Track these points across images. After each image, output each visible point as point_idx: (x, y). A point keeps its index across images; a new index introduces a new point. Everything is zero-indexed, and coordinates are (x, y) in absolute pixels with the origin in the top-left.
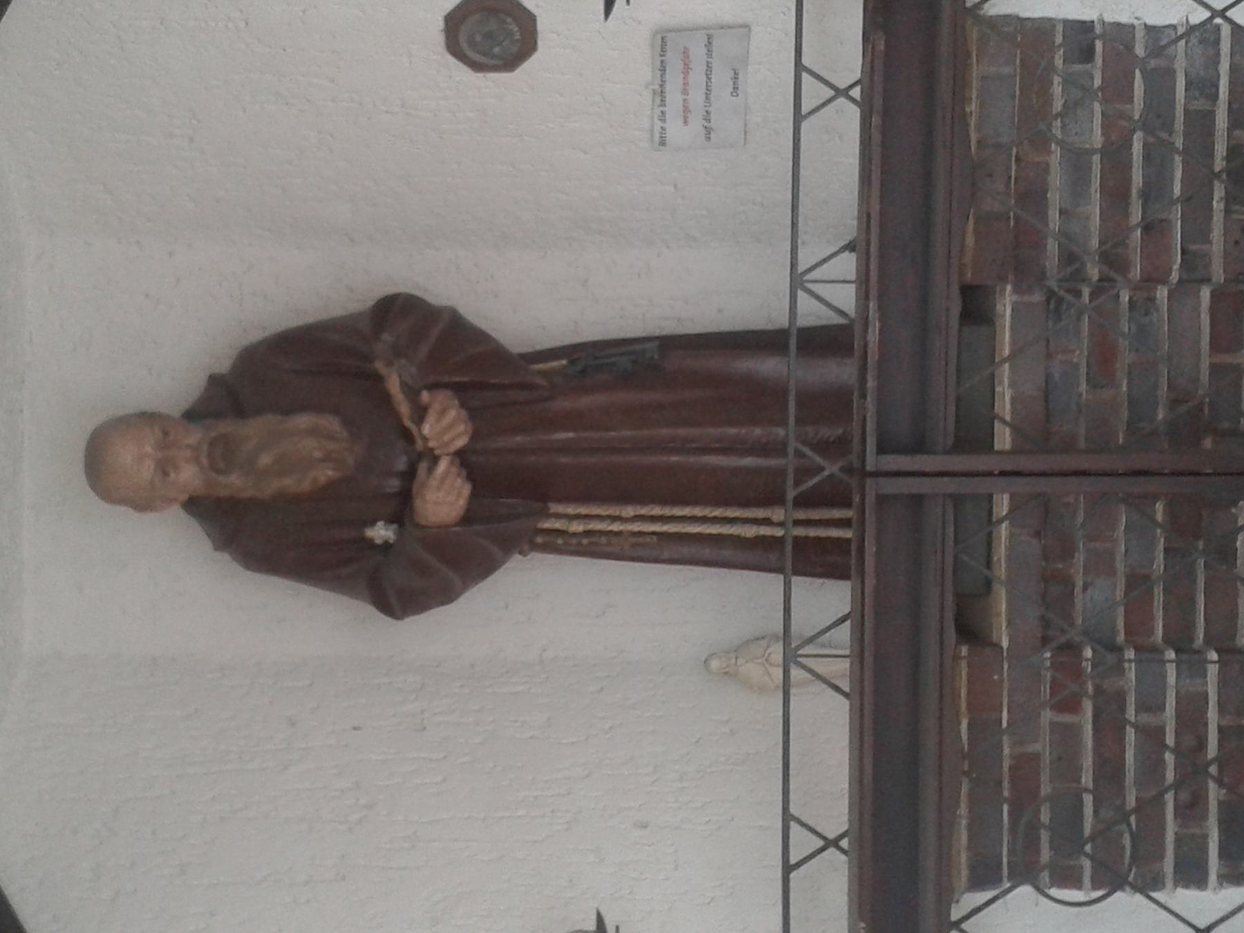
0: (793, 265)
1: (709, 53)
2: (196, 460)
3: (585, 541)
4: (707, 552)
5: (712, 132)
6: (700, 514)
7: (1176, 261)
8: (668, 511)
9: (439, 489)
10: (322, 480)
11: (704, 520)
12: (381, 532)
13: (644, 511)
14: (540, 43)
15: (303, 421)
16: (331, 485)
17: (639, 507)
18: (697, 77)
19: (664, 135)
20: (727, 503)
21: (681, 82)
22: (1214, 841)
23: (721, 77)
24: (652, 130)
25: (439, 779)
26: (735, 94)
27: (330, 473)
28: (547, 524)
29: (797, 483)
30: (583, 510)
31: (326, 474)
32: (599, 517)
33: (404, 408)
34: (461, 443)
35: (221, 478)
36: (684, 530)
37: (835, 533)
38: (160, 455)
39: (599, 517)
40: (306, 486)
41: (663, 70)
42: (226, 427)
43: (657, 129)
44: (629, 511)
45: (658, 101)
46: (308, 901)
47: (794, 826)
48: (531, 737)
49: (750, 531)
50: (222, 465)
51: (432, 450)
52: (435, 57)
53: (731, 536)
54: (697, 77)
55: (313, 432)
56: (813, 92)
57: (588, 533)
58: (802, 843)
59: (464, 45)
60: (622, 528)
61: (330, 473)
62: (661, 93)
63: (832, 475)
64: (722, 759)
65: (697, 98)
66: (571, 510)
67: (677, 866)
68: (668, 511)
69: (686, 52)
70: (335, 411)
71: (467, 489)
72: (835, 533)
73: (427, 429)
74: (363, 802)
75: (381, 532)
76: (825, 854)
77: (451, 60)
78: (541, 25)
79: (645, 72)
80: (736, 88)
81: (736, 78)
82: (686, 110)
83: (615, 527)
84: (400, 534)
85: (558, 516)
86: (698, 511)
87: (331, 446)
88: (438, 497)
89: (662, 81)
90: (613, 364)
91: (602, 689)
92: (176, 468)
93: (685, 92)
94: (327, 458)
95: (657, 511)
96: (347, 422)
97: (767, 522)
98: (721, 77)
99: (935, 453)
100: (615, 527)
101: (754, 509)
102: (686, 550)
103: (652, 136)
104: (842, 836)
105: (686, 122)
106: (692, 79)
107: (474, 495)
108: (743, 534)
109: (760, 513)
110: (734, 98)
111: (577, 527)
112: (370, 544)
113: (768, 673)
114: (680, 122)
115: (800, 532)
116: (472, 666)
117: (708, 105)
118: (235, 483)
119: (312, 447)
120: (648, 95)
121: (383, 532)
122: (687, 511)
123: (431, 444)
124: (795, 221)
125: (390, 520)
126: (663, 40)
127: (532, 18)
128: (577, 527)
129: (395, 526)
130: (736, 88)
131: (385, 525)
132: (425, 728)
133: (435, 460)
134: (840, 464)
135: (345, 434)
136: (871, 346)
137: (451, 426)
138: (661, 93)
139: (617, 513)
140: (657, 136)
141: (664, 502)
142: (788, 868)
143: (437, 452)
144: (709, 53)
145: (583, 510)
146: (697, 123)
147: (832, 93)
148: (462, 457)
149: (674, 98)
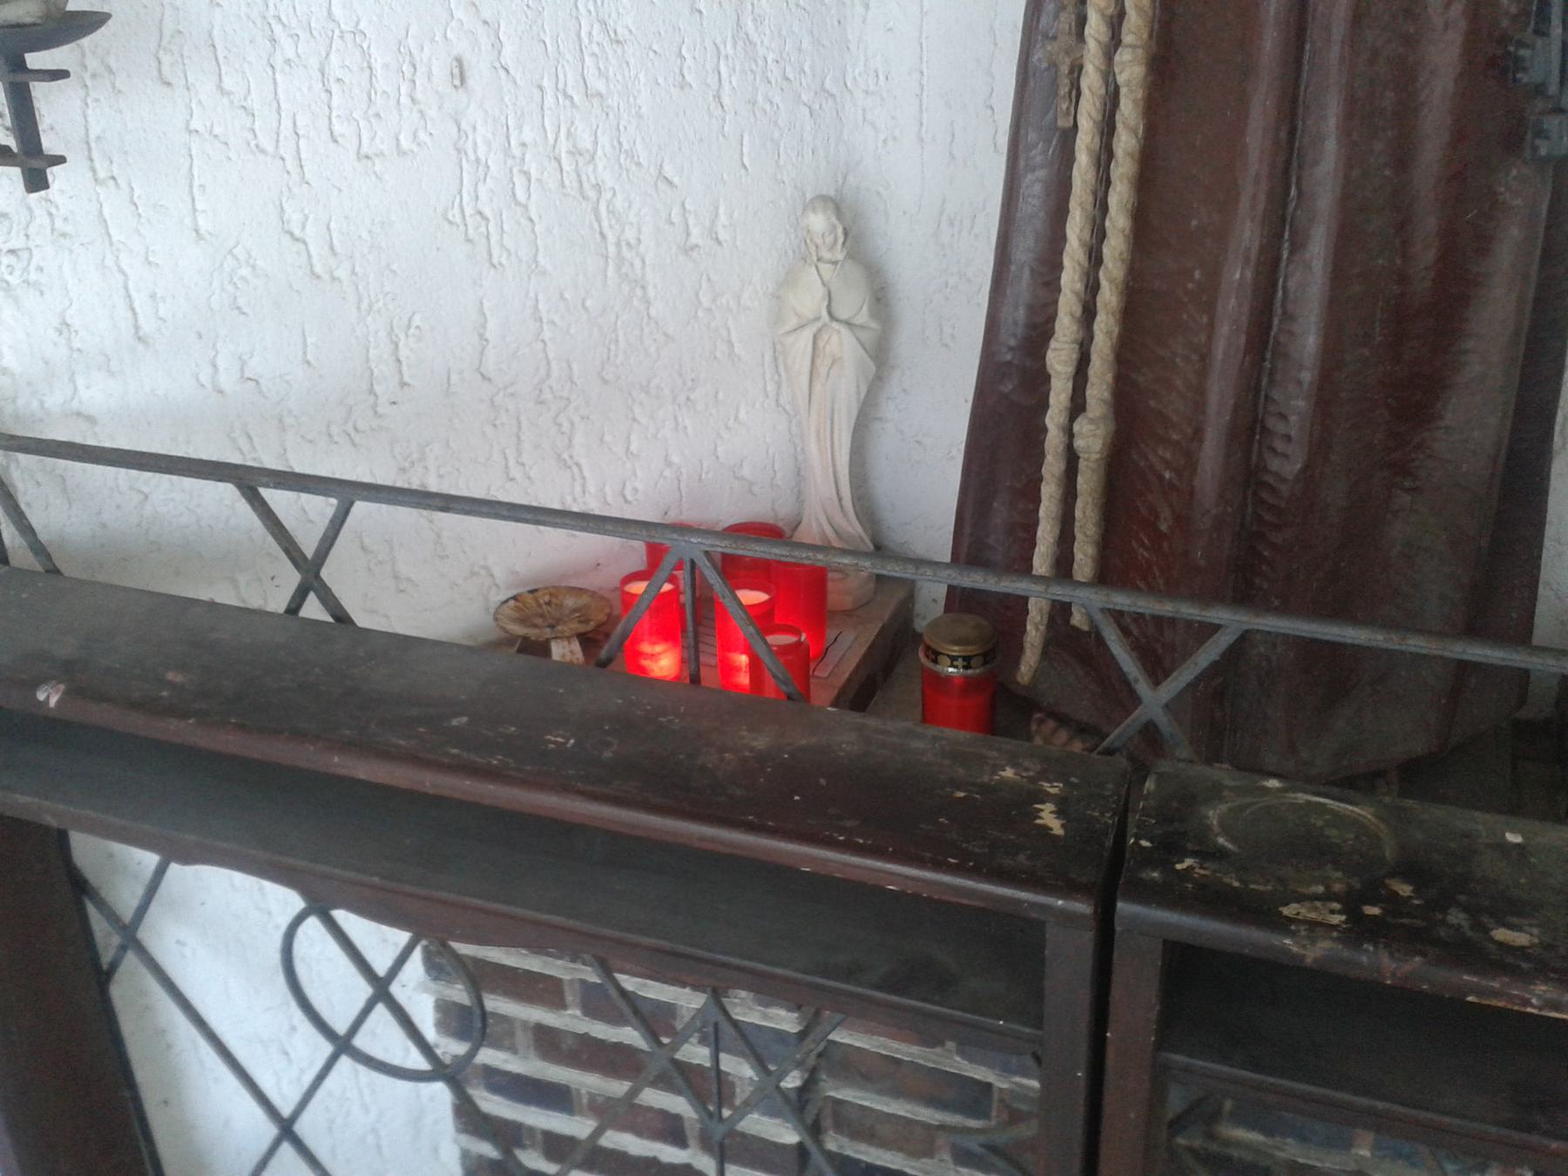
4: (1025, 250)
6: (1107, 251)
7: (1500, 1001)
11: (1095, 258)
13: (1129, 111)
17: (1140, 94)
20: (1130, 313)
22: (506, 1061)
36: (1074, 204)
37: (1046, 534)
49: (1059, 359)
60: (1092, 45)
63: (1136, 700)
64: (630, 234)
67: (28, 284)
68: (1123, 169)
72: (1046, 534)
86: (1115, 247)
90: (1542, 32)
95: (1126, 142)
97: (1077, 406)
99: (1160, 1046)
101: (1109, 377)
102: (1034, 186)
104: (329, 600)
108: (1053, 344)
109: (1099, 390)
113: (802, 327)
122: (1118, 221)
134: (1163, 721)
139: (1128, 38)
141: (1148, 158)
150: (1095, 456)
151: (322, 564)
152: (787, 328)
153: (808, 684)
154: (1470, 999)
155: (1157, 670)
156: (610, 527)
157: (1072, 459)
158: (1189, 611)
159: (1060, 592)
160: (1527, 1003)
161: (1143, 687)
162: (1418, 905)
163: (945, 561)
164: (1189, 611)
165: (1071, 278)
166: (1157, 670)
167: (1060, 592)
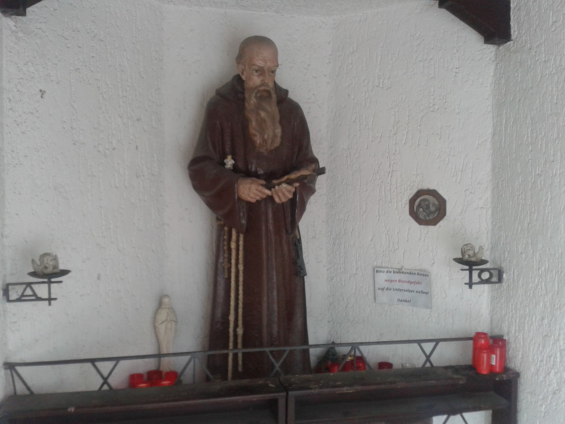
0: (362, 344)
1: (417, 292)
2: (262, 85)
3: (225, 248)
4: (220, 299)
5: (382, 291)
8: (241, 283)
9: (257, 190)
10: (256, 139)
12: (229, 162)
14: (423, 226)
15: (279, 131)
16: (253, 143)
18: (406, 286)
19: (381, 272)
21: (405, 280)
23: (407, 296)
24: (381, 267)
25: (117, 185)
26: (399, 300)
27: (258, 142)
28: (234, 232)
29: (271, 352)
30: (241, 248)
31: (258, 140)
32: (237, 254)
33: (293, 176)
34: (277, 200)
35: (254, 94)
38: (265, 69)
39: (237, 254)
40: (252, 131)
41: (410, 273)
42: (274, 96)
43: (383, 270)
44: (241, 267)
45: (396, 270)
46: (64, 128)
47: (114, 363)
48: (134, 224)
49: (232, 318)
50: (258, 95)
51: (274, 187)
52: (416, 185)
53: (229, 309)
54: (406, 286)
55: (275, 136)
56: (428, 347)
57: (230, 249)
58: (105, 367)
59: (422, 197)
61: (258, 142)
62: (400, 271)
65: (397, 285)
66: (241, 243)
68: (241, 283)
69: (419, 283)
70: (282, 143)
71: (253, 201)
73: (284, 185)
74: (107, 152)
75: (229, 162)
76: (99, 376)
77: (414, 191)
78: (431, 228)
79: (408, 265)
80: (401, 301)
81: (406, 301)
82: (391, 281)
83: (233, 261)
84: (229, 170)
85: (238, 238)
86: (241, 297)
87: (269, 142)
88: (253, 189)
89: (405, 273)
91: (153, 251)
92: (259, 75)
93: (399, 281)
94: (265, 141)
96: (277, 149)
97: (236, 326)
98: (407, 296)
100: (233, 261)
103: (379, 267)
104: (109, 385)
105: (386, 281)
106: (406, 284)
107: (249, 203)
109: (240, 323)
110: (397, 300)
111: (233, 245)
112: (225, 157)
113: (163, 322)
114: (387, 279)
115: (240, 346)
116: (161, 196)
117: (394, 290)
118: (252, 101)
119: (268, 135)
120: (399, 266)
121: (230, 163)
122: (241, 292)
123: (277, 187)
124: (380, 343)
125: (234, 165)
126: (425, 274)
127: (435, 225)
128: (233, 245)
129: (232, 168)
130: (401, 301)
131: (233, 164)
132: (137, 177)
133: (270, 189)
134: (280, 371)
135: (273, 148)
136: (342, 389)
137: (284, 194)
138: (400, 271)
140: (381, 269)
142: (92, 361)
143: (273, 189)
144: (417, 292)
145: (241, 248)
146: (386, 285)
147: (428, 354)
148: (270, 198)
149: (397, 277)
150: (241, 335)
151: (426, 360)
152: (159, 323)
153: (411, 340)
154: (337, 392)
155: (277, 359)
156: (171, 355)
157: (236, 336)
158: (282, 348)
159: (235, 351)
160: (344, 391)
161: (276, 364)
162: (296, 375)
163: (11, 286)
164: (282, 348)
165: (232, 303)
166: (277, 359)
167: (235, 351)
